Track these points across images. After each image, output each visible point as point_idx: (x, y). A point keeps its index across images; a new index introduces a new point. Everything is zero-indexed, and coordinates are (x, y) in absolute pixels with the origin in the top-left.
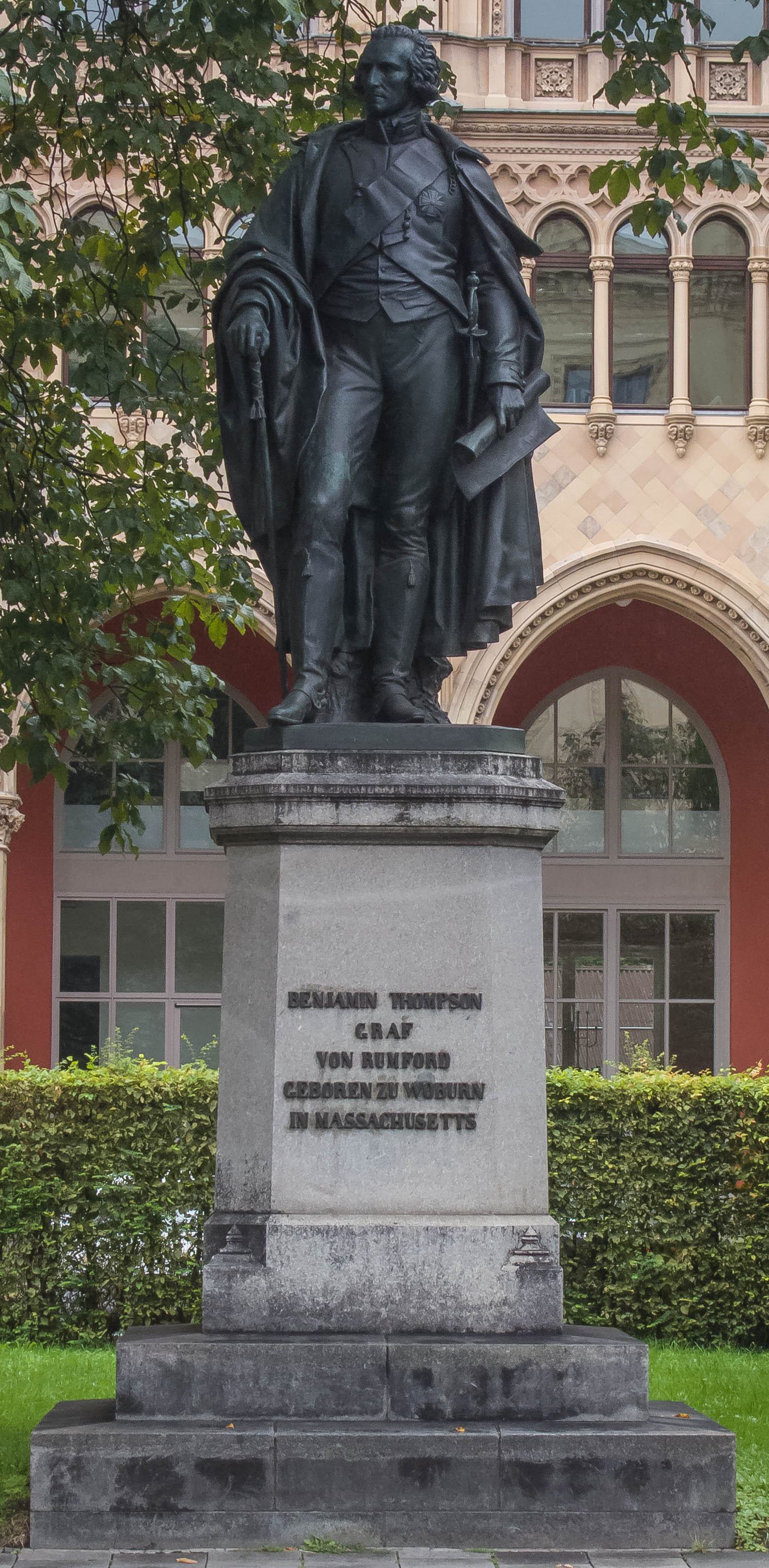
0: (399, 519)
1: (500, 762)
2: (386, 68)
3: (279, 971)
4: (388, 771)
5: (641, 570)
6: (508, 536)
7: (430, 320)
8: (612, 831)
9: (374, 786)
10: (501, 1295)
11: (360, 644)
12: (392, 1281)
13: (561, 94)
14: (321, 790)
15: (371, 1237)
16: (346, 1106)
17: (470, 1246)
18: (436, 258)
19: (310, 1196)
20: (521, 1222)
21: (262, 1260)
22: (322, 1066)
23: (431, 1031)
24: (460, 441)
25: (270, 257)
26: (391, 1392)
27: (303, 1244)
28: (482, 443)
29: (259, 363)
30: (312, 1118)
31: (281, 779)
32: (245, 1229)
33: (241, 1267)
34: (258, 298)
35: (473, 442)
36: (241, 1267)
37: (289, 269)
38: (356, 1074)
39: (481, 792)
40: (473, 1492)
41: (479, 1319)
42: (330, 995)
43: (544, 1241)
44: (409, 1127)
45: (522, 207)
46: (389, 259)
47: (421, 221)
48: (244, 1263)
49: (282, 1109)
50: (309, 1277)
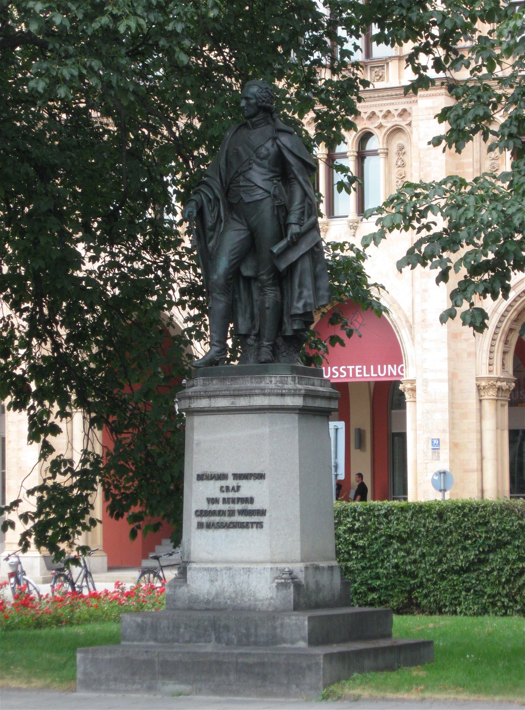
1: (273, 379)
10: (270, 595)
12: (231, 589)
15: (224, 572)
16: (216, 519)
17: (259, 575)
18: (265, 174)
19: (204, 555)
22: (209, 503)
23: (248, 488)
27: (200, 575)
28: (280, 249)
30: (205, 524)
38: (221, 506)
40: (227, 674)
41: (262, 605)
47: (258, 160)
49: (195, 520)
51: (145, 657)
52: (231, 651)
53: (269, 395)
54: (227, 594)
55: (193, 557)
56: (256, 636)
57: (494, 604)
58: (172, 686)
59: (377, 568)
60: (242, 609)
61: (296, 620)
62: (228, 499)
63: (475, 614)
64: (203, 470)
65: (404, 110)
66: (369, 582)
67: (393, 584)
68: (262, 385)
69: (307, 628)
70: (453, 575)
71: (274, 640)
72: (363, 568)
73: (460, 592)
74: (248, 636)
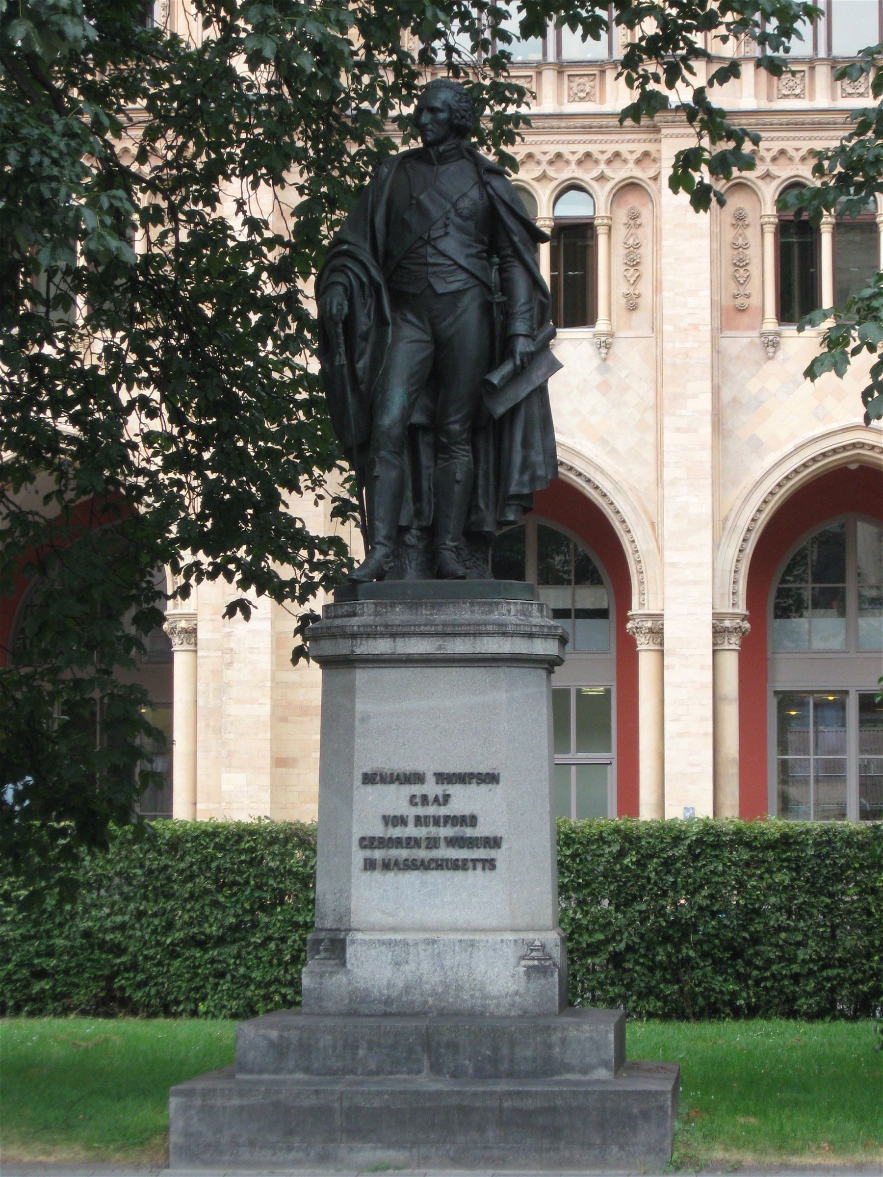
0: (448, 434)
2: (433, 110)
3: (356, 758)
4: (432, 615)
5: (859, 443)
6: (526, 444)
7: (465, 291)
8: (852, 633)
9: (419, 625)
10: (513, 988)
11: (424, 523)
12: (436, 978)
13: (797, 96)
14: (382, 629)
16: (403, 853)
17: (491, 953)
18: (469, 246)
19: (377, 917)
20: (530, 936)
21: (344, 963)
22: (386, 824)
23: (464, 799)
24: (487, 377)
25: (353, 249)
26: (430, 1058)
27: (373, 952)
28: (503, 378)
29: (341, 325)
31: (355, 621)
32: (333, 941)
33: (329, 969)
34: (341, 279)
35: (496, 378)
36: (329, 969)
37: (366, 257)
38: (411, 831)
39: (496, 628)
40: (481, 1129)
41: (498, 1006)
42: (392, 774)
43: (548, 949)
44: (448, 869)
45: (768, 180)
46: (435, 248)
47: (458, 220)
48: (332, 966)
50: (378, 976)
51: (313, 1101)
52: (489, 1089)
53: (513, 635)
54: (428, 986)
55: (356, 920)
56: (512, 1061)
57: (267, 998)
58: (368, 1154)
59: (50, 937)
60: (457, 1014)
61: (592, 1031)
62: (426, 817)
63: (235, 1016)
64: (376, 765)
65: (646, 154)
66: (36, 961)
67: (79, 965)
68: (495, 616)
69: (612, 1046)
70: (193, 949)
71: (547, 1067)
72: (25, 938)
73: (206, 978)
74: (495, 1061)
